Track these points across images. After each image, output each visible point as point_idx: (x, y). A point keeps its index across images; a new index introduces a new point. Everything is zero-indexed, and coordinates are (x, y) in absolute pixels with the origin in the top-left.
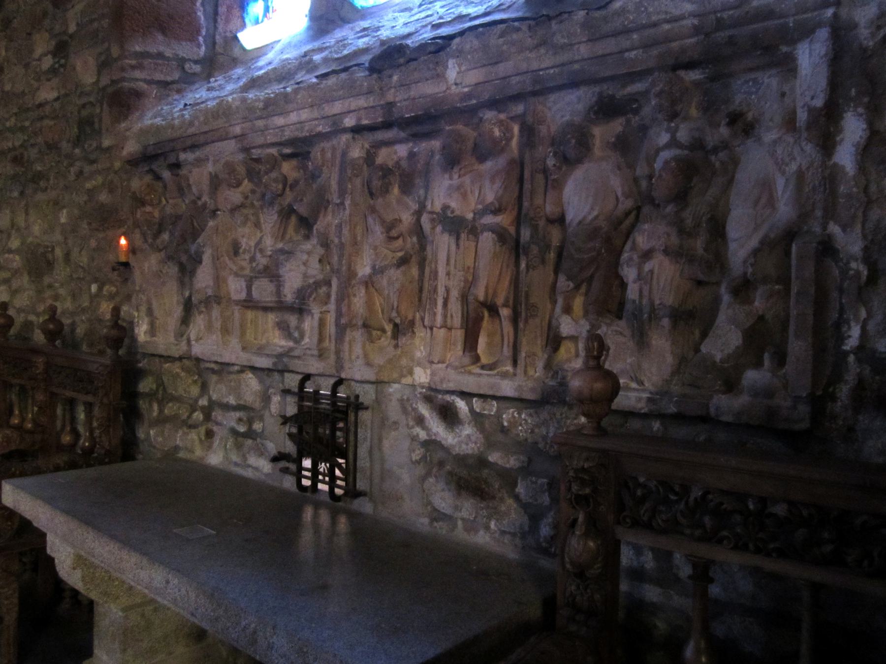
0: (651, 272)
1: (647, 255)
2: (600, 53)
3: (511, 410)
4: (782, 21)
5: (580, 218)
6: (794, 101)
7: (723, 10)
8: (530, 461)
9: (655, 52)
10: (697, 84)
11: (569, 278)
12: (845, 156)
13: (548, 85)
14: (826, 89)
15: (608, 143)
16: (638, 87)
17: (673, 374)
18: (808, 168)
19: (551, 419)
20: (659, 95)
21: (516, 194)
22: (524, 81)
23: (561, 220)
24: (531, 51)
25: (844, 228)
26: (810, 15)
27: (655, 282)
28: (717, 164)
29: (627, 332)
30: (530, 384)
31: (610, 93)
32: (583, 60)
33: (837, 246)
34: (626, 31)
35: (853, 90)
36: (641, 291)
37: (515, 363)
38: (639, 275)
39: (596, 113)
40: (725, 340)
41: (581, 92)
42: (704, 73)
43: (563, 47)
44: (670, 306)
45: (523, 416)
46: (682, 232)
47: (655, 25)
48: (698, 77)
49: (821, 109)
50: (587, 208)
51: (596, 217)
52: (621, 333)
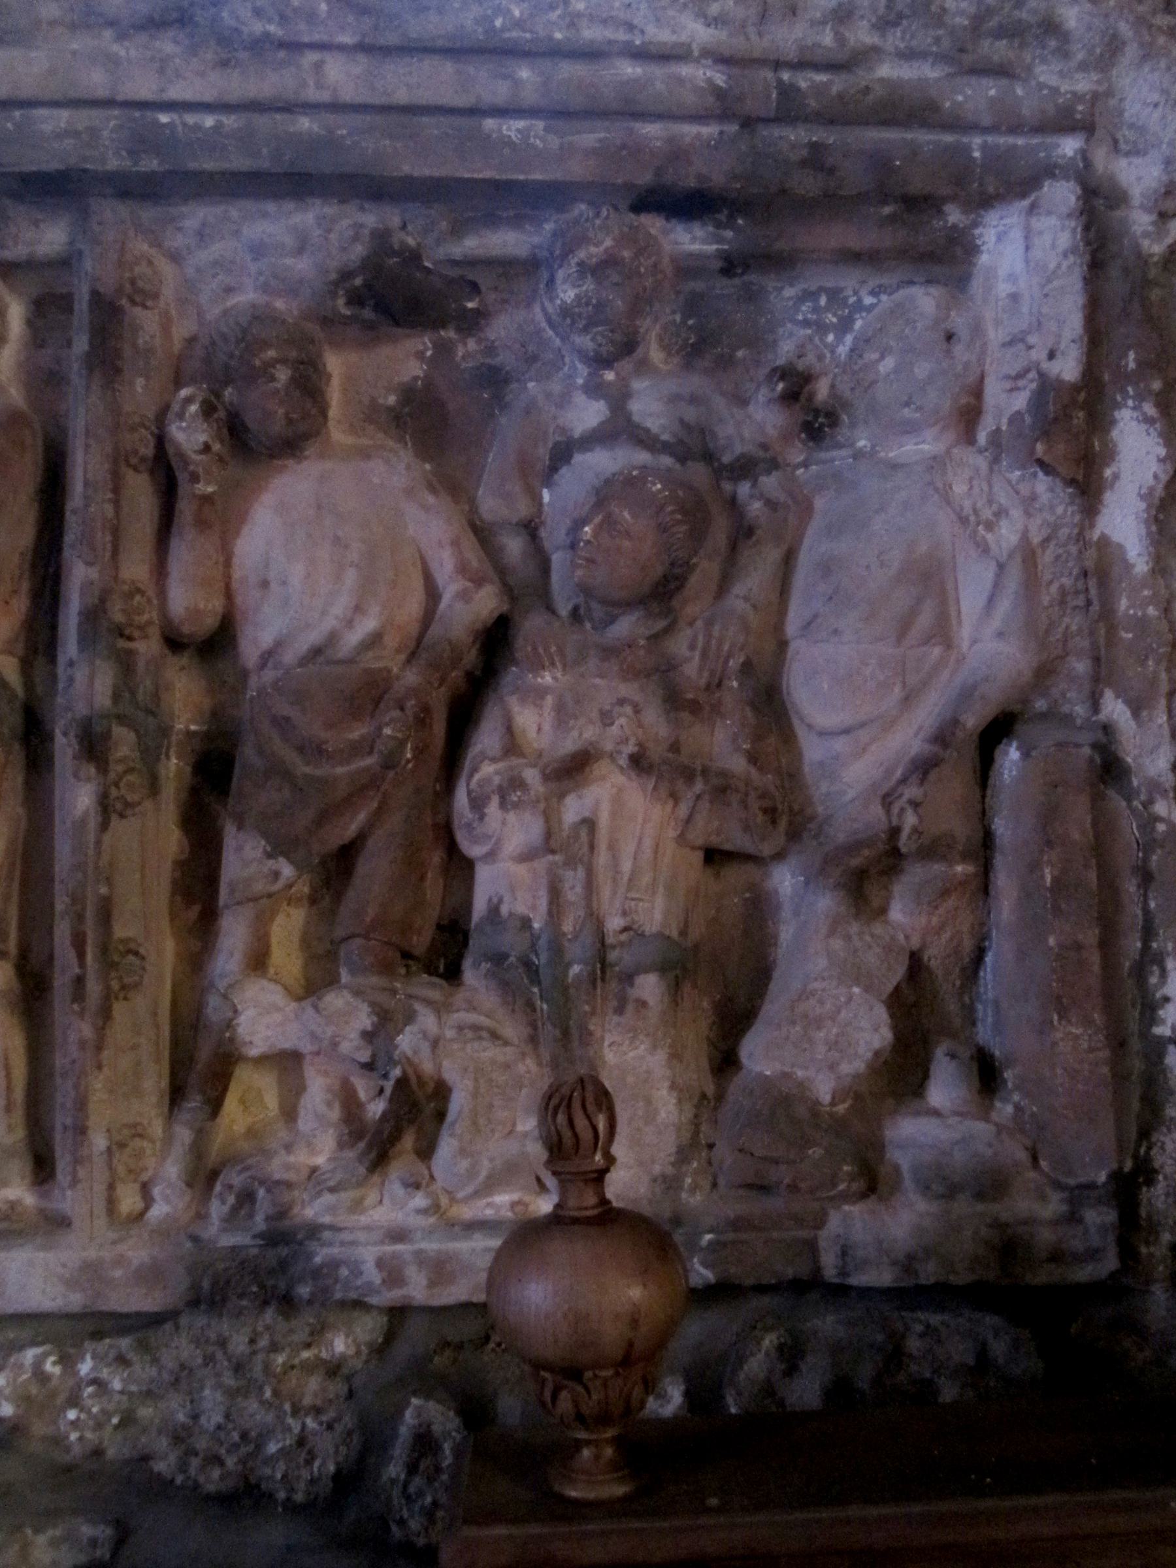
0: (590, 824)
1: (574, 769)
2: (402, 96)
3: (30, 1354)
4: (948, 138)
5: (314, 637)
6: (981, 361)
7: (801, 65)
8: (123, 1535)
9: (590, 137)
10: (688, 268)
11: (280, 847)
12: (1124, 521)
13: (193, 165)
14: (1081, 338)
15: (374, 406)
16: (507, 241)
17: (683, 1155)
18: (1047, 540)
19: (209, 1360)
20: (597, 270)
21: (26, 536)
22: (93, 132)
23: (215, 645)
24: (121, 37)
25: (1137, 708)
26: (1020, 141)
27: (602, 858)
28: (756, 507)
29: (512, 1030)
30: (138, 1252)
31: (411, 241)
32: (336, 107)
33: (1121, 754)
34: (499, 51)
35: (1132, 355)
36: (555, 893)
37: (42, 1167)
38: (548, 835)
39: (356, 299)
40: (824, 1025)
41: (307, 217)
42: (720, 240)
43: (260, 46)
44: (660, 936)
45: (85, 1367)
46: (675, 701)
47: (592, 54)
48: (696, 247)
49: (1076, 388)
50: (341, 606)
51: (374, 640)
52: (495, 1036)
